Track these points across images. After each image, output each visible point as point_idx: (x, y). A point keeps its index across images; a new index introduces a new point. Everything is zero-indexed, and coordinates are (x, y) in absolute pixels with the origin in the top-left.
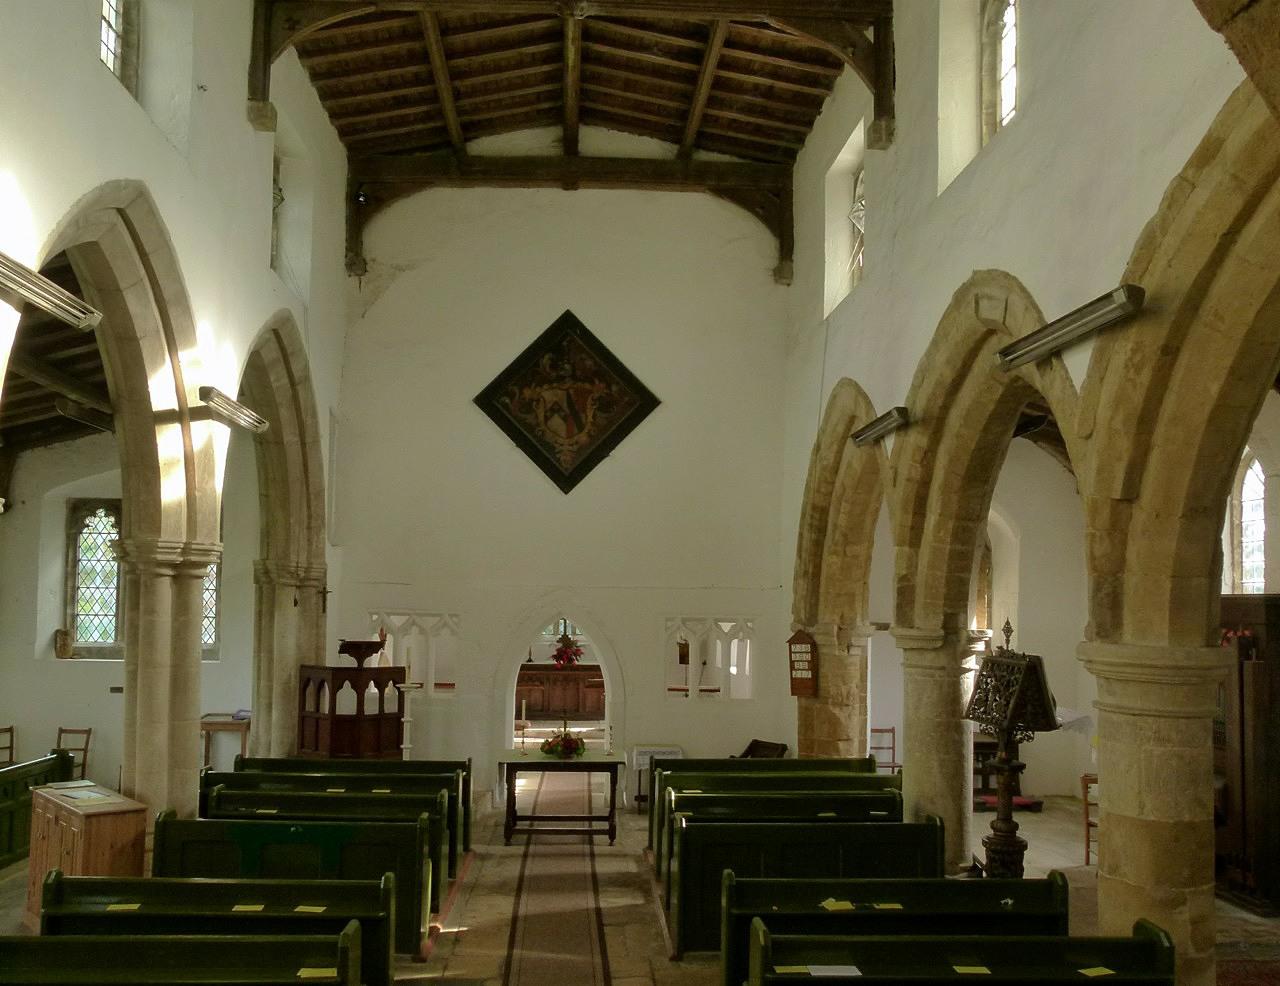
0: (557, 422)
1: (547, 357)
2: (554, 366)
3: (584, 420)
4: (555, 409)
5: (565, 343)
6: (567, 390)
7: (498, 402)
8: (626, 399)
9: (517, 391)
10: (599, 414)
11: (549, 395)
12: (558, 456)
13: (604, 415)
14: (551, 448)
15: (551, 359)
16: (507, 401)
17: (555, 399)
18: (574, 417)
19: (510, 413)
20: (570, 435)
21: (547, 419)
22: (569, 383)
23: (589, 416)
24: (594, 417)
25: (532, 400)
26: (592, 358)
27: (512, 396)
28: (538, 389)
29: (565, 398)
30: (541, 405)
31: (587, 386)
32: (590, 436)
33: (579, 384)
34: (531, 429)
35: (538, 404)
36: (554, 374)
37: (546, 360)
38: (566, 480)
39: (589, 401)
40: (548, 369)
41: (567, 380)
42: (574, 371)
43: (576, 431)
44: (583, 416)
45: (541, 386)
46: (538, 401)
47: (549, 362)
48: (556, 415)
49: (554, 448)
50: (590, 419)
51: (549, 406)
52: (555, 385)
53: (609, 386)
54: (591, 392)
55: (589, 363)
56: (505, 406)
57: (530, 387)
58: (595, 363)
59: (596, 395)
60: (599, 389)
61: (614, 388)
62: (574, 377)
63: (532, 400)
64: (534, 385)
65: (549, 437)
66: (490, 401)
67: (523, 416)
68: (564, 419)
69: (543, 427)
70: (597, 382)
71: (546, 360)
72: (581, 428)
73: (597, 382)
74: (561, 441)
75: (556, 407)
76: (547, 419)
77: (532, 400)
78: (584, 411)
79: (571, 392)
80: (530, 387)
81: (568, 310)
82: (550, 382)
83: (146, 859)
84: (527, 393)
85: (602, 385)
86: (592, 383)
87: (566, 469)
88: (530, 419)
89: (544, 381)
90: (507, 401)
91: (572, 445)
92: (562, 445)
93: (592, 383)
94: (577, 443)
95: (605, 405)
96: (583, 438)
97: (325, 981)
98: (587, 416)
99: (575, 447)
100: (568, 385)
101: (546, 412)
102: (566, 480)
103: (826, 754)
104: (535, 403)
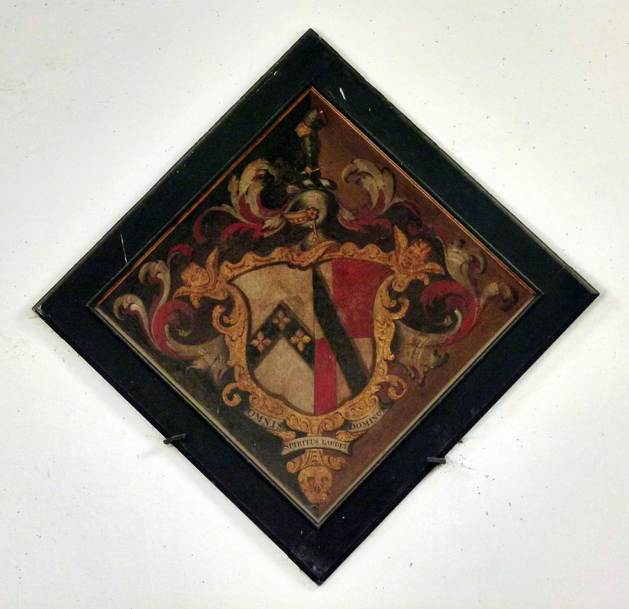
0: (285, 366)
1: (250, 173)
2: (272, 198)
3: (367, 360)
4: (278, 327)
5: (303, 130)
6: (314, 266)
7: (109, 311)
8: (493, 288)
9: (165, 277)
10: (409, 334)
11: (263, 285)
12: (291, 467)
13: (424, 340)
14: (269, 444)
15: (265, 178)
16: (137, 306)
17: (279, 296)
18: (336, 349)
19: (305, 501)
20: (325, 401)
21: (254, 356)
22: (317, 246)
23: (377, 348)
24: (396, 345)
25: (214, 303)
26: (385, 169)
27: (149, 291)
28: (226, 270)
29: (307, 295)
30: (238, 317)
31: (372, 252)
32: (385, 403)
33: (350, 248)
34: (208, 386)
35: (227, 313)
36: (273, 222)
37: (247, 184)
38: (319, 543)
39: (381, 299)
40: (255, 209)
41: (311, 238)
42: (333, 206)
43: (343, 390)
44: (362, 345)
45: (235, 261)
46: (229, 304)
47: (259, 188)
48: (282, 345)
49: (279, 443)
50: (385, 351)
51: (260, 318)
52: (276, 254)
53: (438, 254)
54: (386, 271)
55: (376, 184)
56: (131, 321)
57: (203, 265)
58: (398, 186)
59: (401, 281)
60: (408, 261)
61: (455, 257)
62: (331, 228)
63: (208, 304)
64: (212, 257)
65: (261, 413)
66: (77, 309)
67: (186, 350)
68: (308, 354)
69: (245, 383)
70: (401, 239)
71: (247, 184)
72: (358, 381)
73: (401, 239)
74: (298, 421)
75: (283, 321)
76: (254, 356)
77: (214, 303)
78: (368, 332)
79: (327, 272)
80: (203, 265)
81: (311, 31)
82: (262, 246)
83: (238, 160)
84: (196, 281)
85: (420, 250)
86: (387, 244)
87: (316, 509)
88: (205, 358)
89: (251, 242)
90: (137, 306)
91: (331, 433)
92: (300, 434)
93: (387, 244)
94: (347, 425)
95: (426, 310)
96: (366, 411)
97: (164, 178)
98: (374, 346)
99: (341, 442)
100: (310, 257)
101: (251, 337)
102: (319, 543)
103: (101, 305)
104: (218, 311)
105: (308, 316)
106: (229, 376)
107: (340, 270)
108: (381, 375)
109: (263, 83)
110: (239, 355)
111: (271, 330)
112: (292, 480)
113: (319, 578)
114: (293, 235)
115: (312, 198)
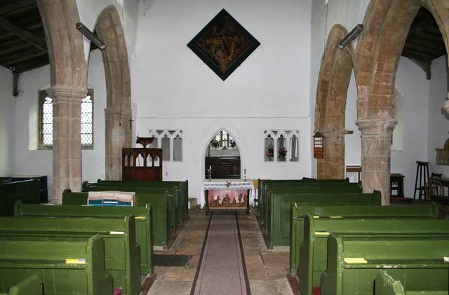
0: (220, 53)
4: (218, 48)
16: (200, 45)
18: (226, 50)
20: (225, 58)
27: (201, 43)
31: (231, 38)
37: (215, 29)
42: (226, 31)
53: (240, 38)
60: (236, 39)
61: (242, 39)
68: (222, 51)
71: (215, 29)
76: (215, 51)
86: (233, 37)
93: (233, 37)
96: (230, 58)
105: (223, 46)
106: (212, 54)
107: (227, 40)
108: (232, 54)
109: (117, 45)
110: (213, 51)
111: (217, 48)
112: (220, 68)
113: (223, 10)
114: (221, 36)
115: (223, 31)
